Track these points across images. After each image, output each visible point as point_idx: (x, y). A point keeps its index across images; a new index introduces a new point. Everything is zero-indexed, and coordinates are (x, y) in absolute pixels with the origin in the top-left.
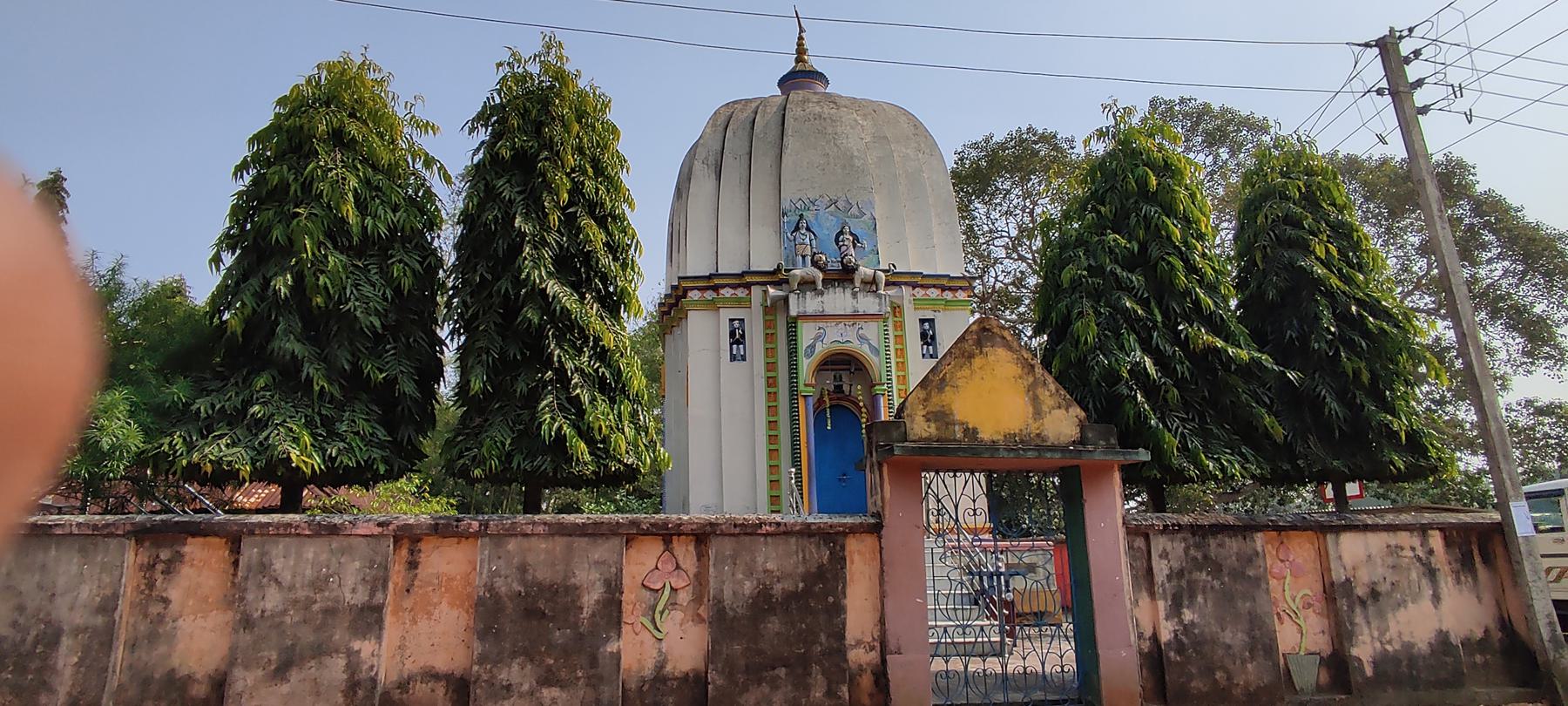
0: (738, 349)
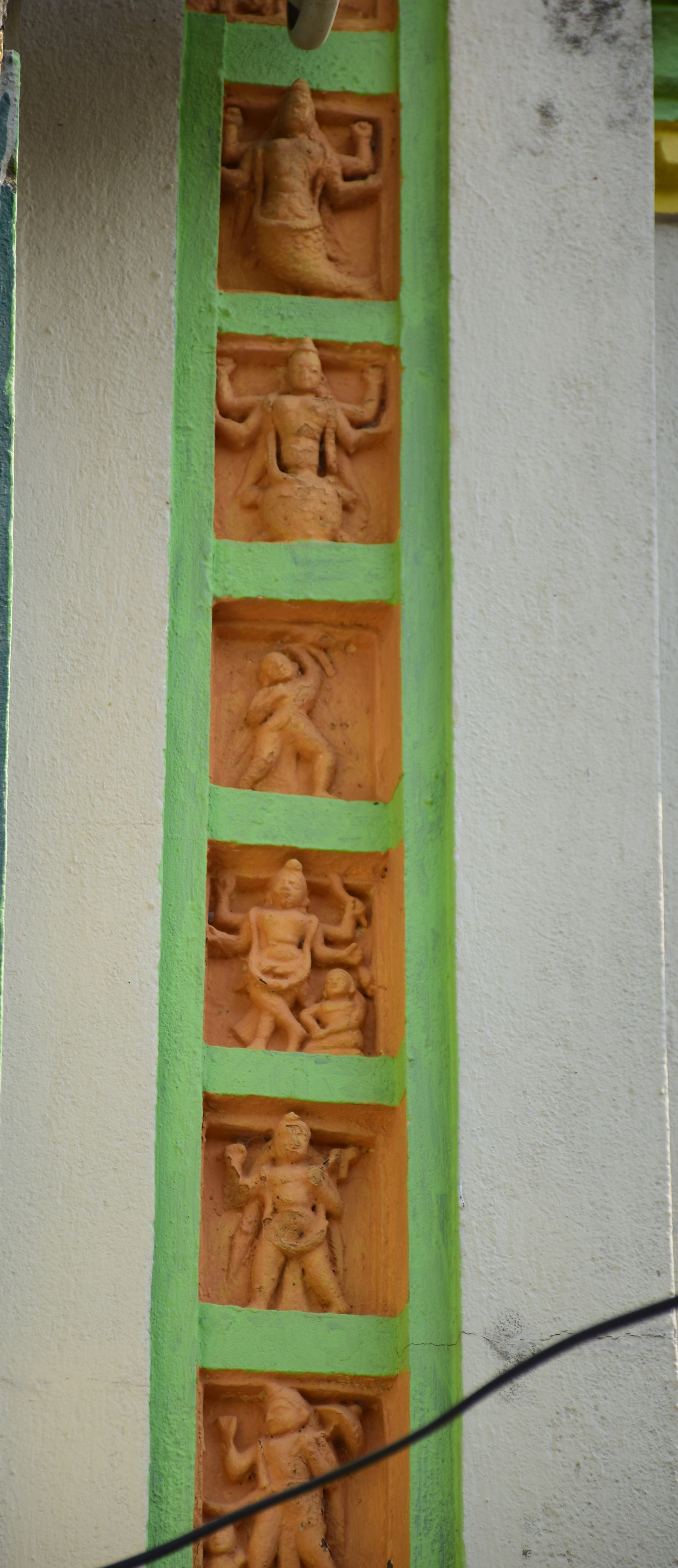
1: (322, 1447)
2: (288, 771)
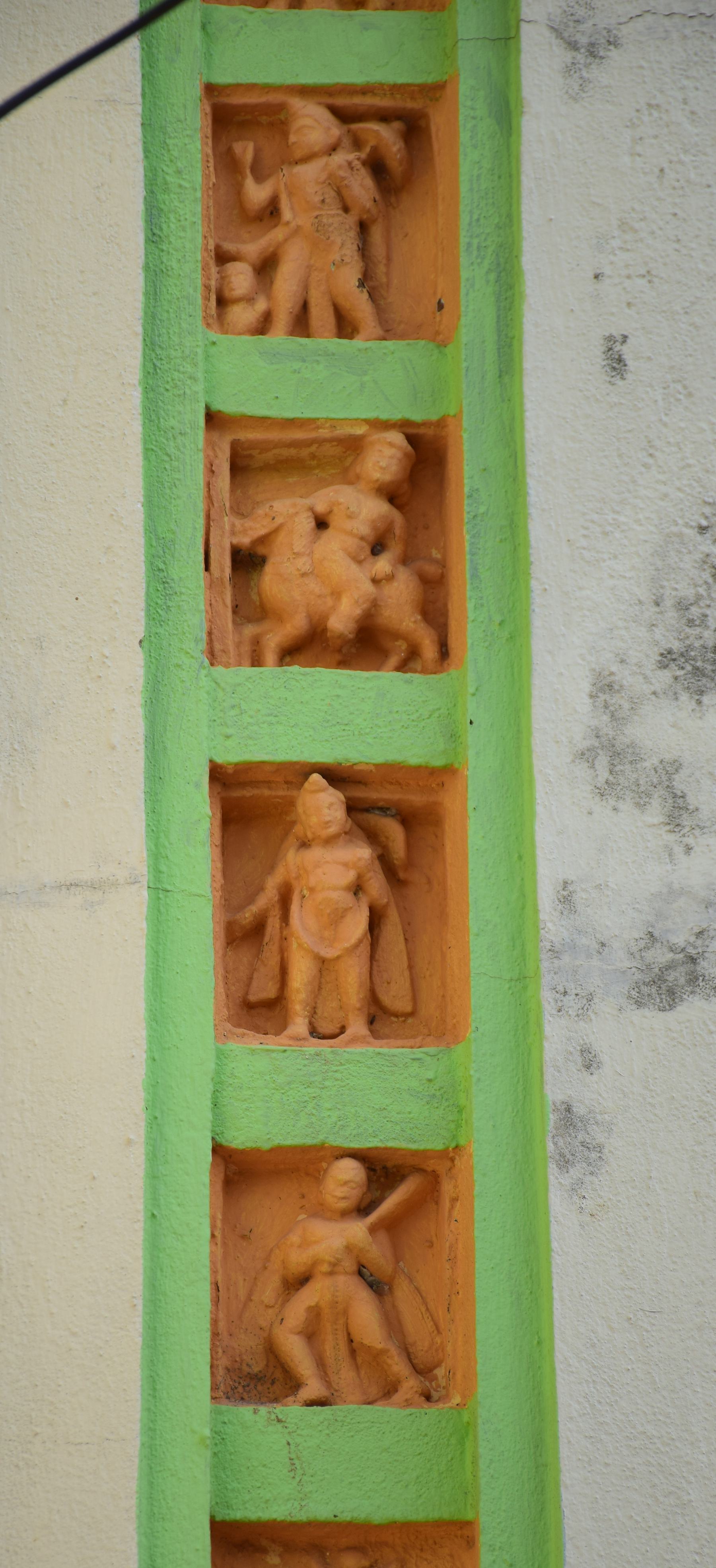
1: (356, 172)
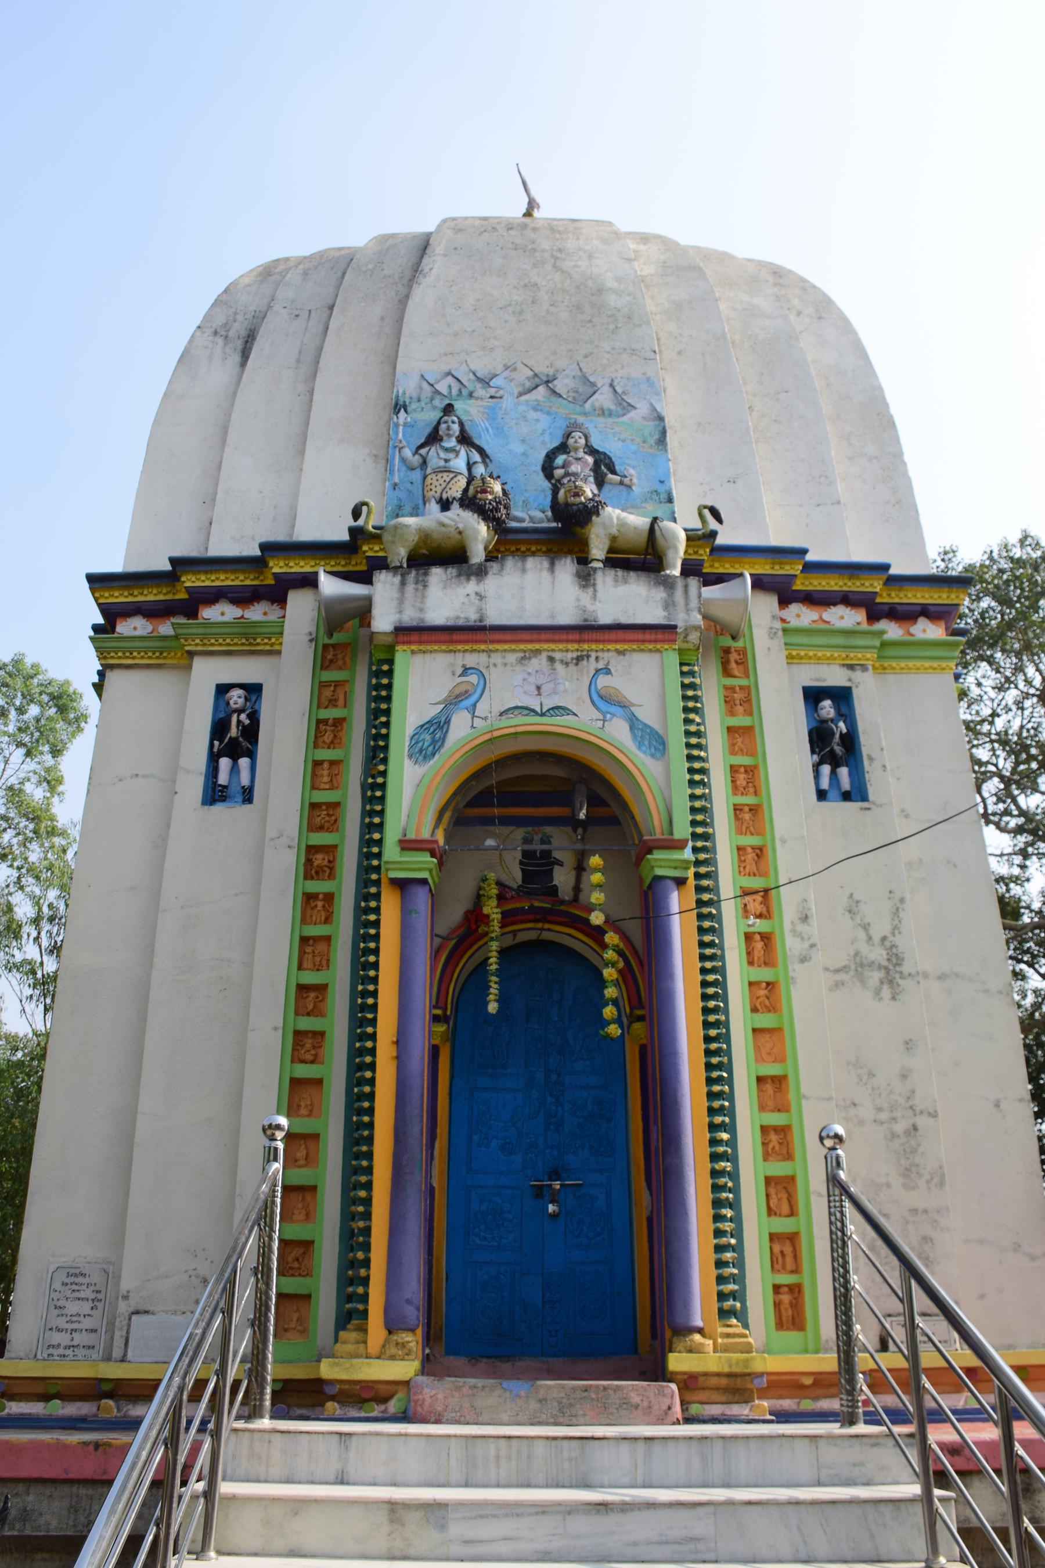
0: (235, 769)
2: (740, 752)
